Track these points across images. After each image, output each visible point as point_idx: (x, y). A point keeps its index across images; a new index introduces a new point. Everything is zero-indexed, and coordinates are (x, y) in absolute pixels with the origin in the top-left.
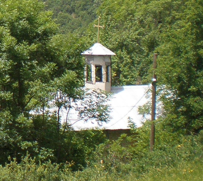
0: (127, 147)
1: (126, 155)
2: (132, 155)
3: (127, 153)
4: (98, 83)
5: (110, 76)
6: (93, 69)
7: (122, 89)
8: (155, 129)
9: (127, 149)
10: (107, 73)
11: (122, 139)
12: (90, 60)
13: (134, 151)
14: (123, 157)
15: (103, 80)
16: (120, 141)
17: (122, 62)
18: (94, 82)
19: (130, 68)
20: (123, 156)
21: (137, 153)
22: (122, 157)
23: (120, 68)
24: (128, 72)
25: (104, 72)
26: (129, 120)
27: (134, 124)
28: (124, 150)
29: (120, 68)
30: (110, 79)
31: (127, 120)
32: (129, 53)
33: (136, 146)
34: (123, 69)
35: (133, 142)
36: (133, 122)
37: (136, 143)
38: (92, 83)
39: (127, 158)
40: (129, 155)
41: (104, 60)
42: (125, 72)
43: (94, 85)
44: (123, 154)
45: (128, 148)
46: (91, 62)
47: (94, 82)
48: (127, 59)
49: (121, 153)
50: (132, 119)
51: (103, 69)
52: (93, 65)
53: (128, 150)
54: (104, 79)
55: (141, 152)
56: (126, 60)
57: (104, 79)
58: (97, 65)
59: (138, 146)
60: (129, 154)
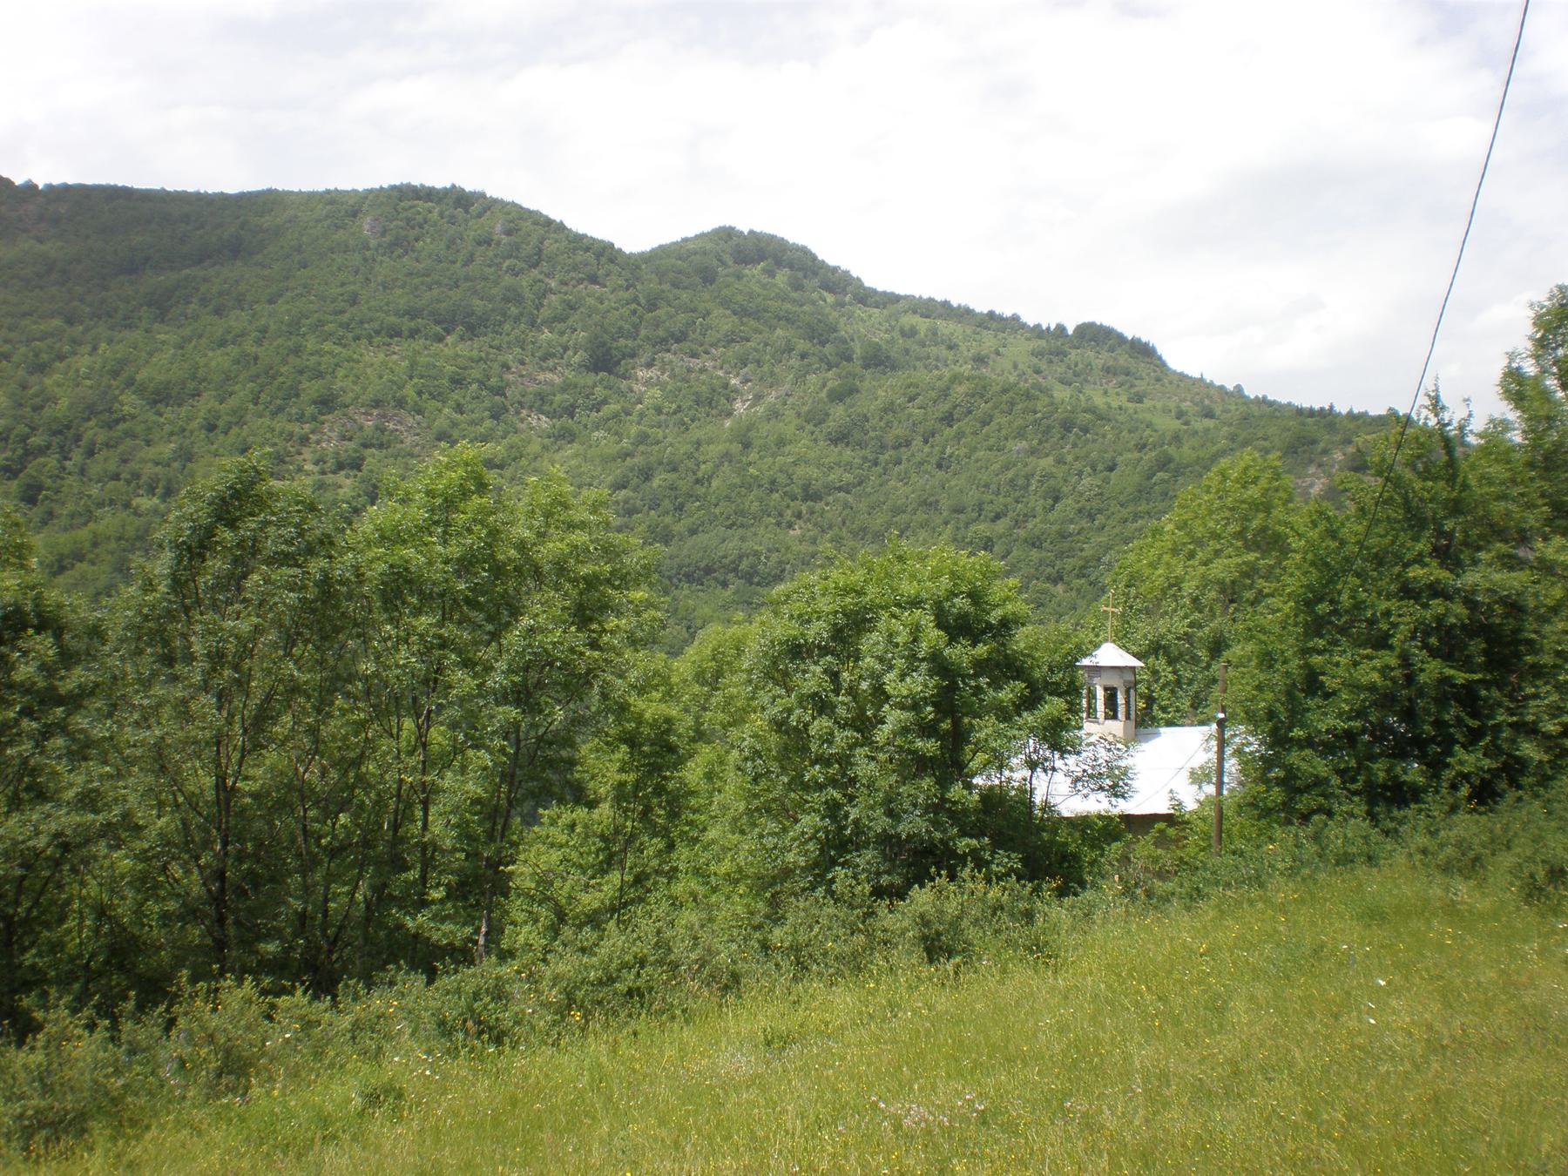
4: (1109, 723)
5: (1133, 708)
6: (1100, 693)
7: (1158, 734)
10: (1128, 703)
17: (1157, 681)
25: (1121, 700)
27: (1180, 804)
31: (1168, 796)
33: (1184, 846)
35: (1178, 840)
46: (1096, 680)
49: (1156, 860)
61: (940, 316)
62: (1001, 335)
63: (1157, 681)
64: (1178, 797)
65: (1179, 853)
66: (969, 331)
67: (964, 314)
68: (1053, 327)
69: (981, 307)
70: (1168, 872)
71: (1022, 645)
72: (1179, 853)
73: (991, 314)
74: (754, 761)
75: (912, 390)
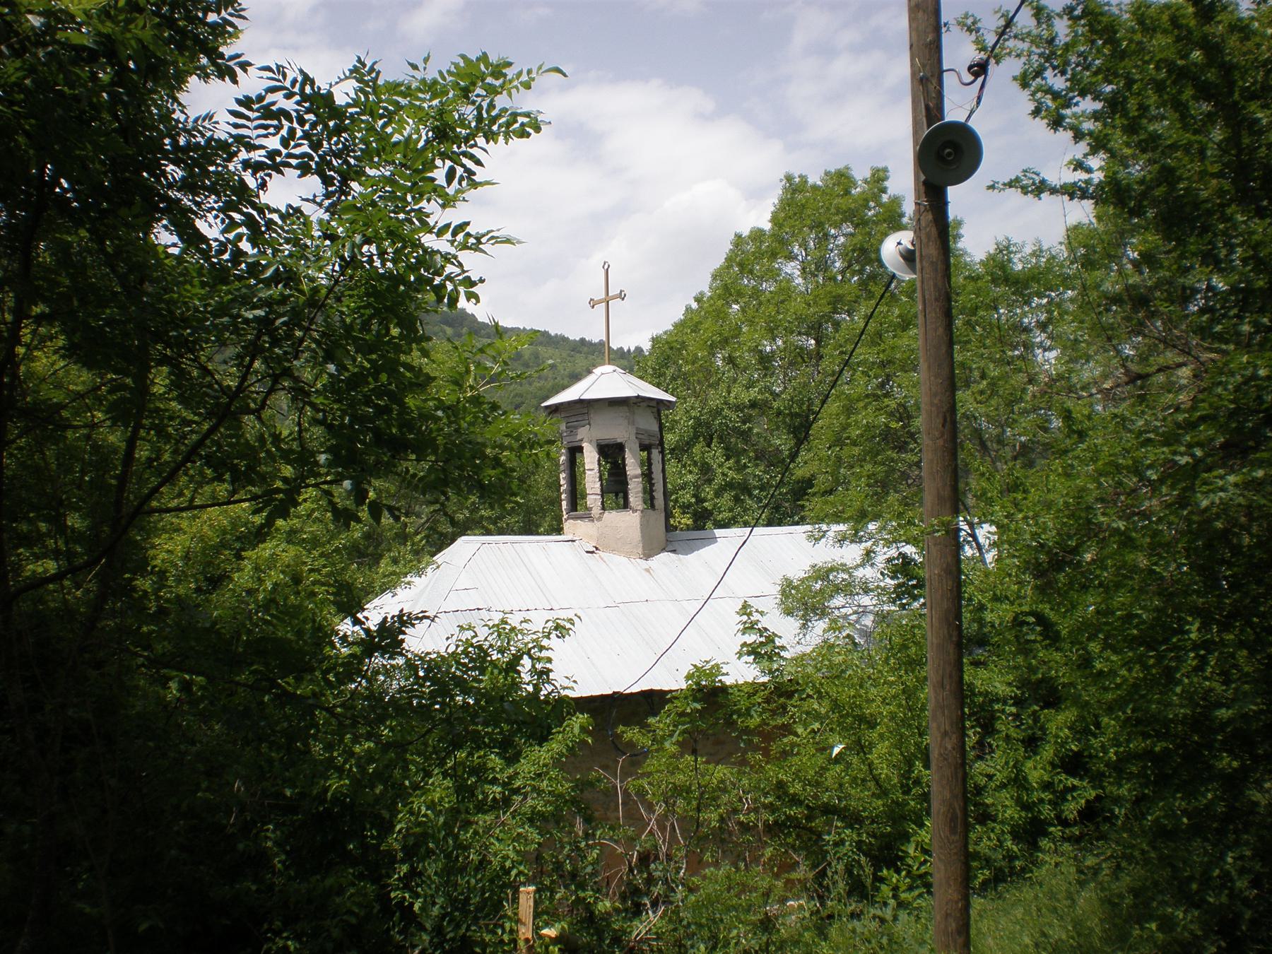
0: (744, 762)
1: (735, 811)
2: (771, 808)
3: (740, 800)
4: (613, 517)
5: (659, 487)
6: (590, 458)
7: (714, 539)
8: (959, 585)
9: (739, 772)
10: (647, 476)
11: (695, 700)
12: (576, 428)
13: (781, 785)
14: (722, 820)
15: (632, 500)
16: (682, 714)
17: (709, 481)
18: (596, 510)
19: (737, 499)
20: (721, 816)
21: (795, 795)
22: (713, 824)
23: (704, 500)
24: (731, 510)
25: (633, 468)
26: (745, 618)
27: (770, 640)
28: (722, 781)
29: (704, 500)
30: (659, 495)
31: (735, 621)
32: (730, 453)
33: (785, 754)
34: (715, 505)
35: (768, 737)
36: (766, 629)
37: (785, 740)
38: (589, 517)
39: (741, 824)
40: (756, 810)
41: (631, 422)
42: (720, 512)
43: (597, 524)
44: (719, 806)
45: (747, 770)
46: (583, 433)
47: (596, 510)
48: (726, 470)
49: (708, 798)
50: (762, 613)
51: (628, 455)
52: (590, 442)
53: (745, 782)
54: (636, 496)
55: (818, 784)
56: (723, 474)
57: (636, 496)
58: (603, 443)
59: (798, 754)
60: (755, 800)
61: (541, 343)
62: (591, 357)
63: (709, 481)
64: (764, 622)
65: (773, 772)
66: (564, 355)
67: (560, 341)
68: (632, 349)
69: (574, 335)
70: (745, 827)
71: (812, 772)
72: (773, 772)
73: (583, 340)
74: (500, 673)
75: (519, 400)
